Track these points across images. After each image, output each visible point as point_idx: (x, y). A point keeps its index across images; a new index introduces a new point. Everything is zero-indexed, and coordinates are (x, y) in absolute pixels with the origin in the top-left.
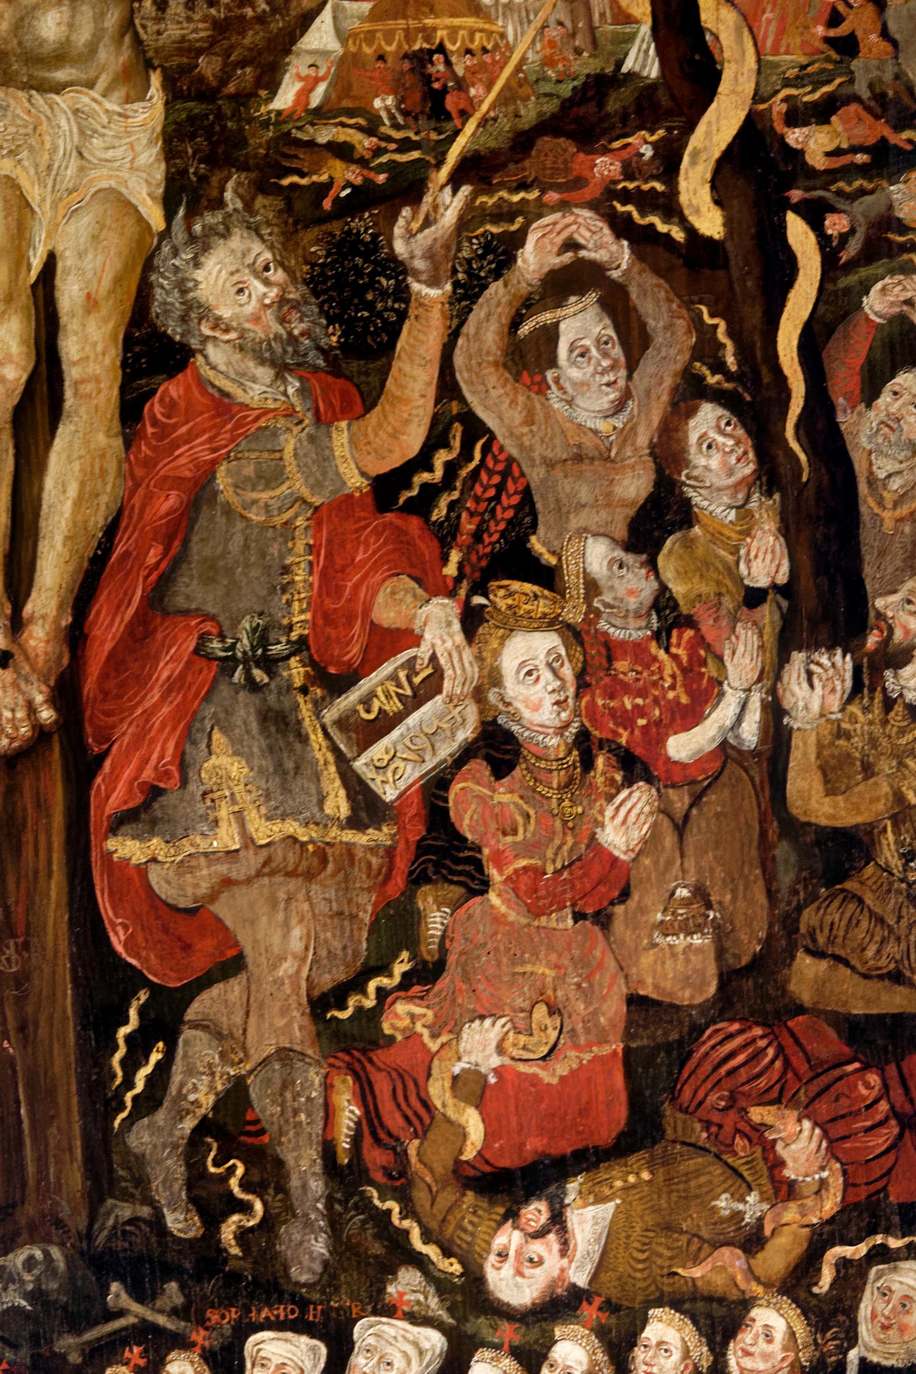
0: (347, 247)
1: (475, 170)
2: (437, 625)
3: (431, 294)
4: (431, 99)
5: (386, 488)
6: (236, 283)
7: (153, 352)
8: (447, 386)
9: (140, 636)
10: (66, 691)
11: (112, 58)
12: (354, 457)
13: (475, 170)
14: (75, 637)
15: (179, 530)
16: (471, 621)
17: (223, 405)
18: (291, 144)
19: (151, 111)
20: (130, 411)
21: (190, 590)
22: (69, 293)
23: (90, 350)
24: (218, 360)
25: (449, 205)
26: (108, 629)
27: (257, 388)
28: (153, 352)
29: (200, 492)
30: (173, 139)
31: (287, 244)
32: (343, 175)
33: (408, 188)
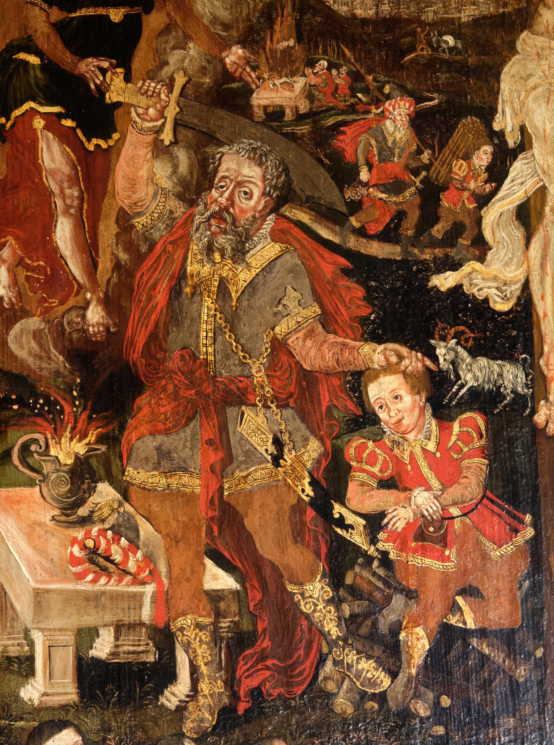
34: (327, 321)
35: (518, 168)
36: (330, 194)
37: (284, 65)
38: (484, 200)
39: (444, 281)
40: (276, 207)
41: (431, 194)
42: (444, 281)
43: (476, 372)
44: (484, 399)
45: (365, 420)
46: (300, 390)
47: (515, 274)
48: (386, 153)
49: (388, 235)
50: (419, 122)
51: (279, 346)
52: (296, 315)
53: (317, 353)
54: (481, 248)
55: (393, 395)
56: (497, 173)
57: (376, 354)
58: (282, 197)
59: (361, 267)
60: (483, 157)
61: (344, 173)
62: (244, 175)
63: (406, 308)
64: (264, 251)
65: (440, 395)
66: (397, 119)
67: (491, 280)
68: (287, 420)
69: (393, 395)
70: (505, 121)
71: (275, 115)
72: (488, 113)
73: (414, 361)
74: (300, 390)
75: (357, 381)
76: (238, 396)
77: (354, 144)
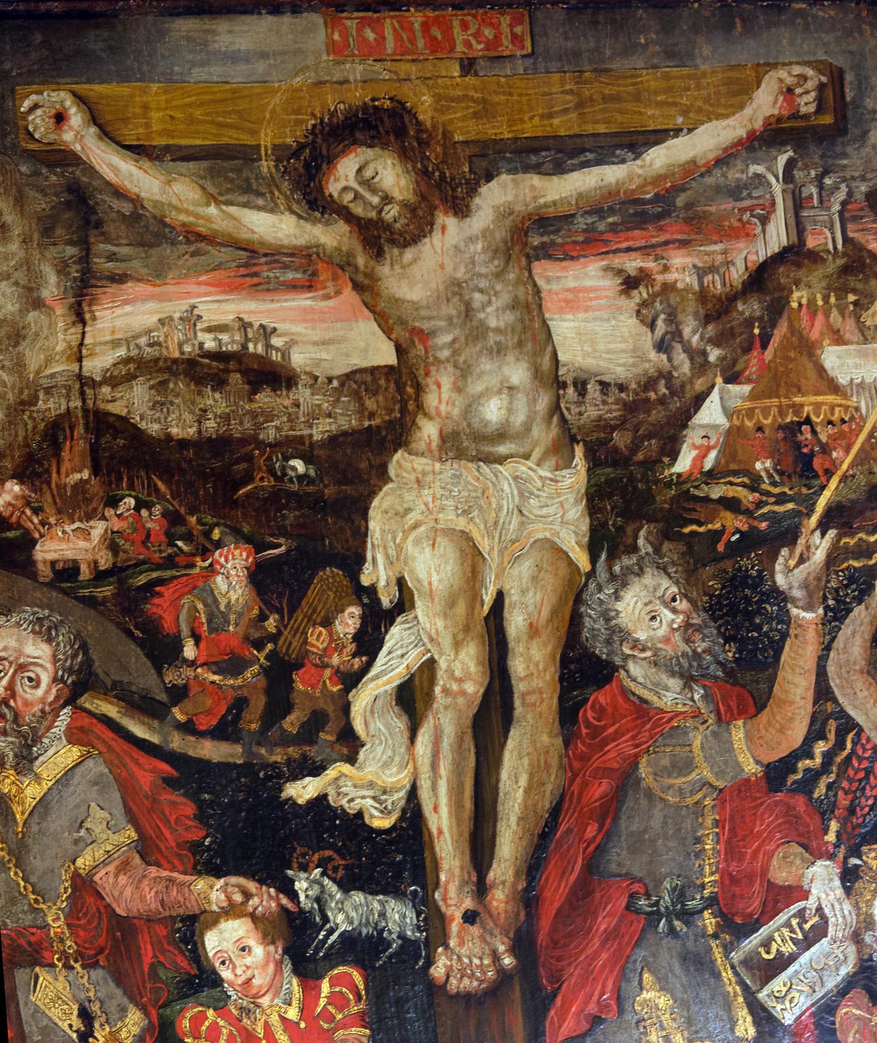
0: (738, 581)
1: (838, 517)
2: (822, 882)
3: (807, 617)
4: (802, 464)
5: (777, 773)
6: (648, 611)
7: (585, 669)
8: (823, 692)
9: (583, 896)
10: (523, 943)
11: (544, 435)
12: (747, 751)
13: (838, 517)
14: (529, 899)
15: (610, 810)
16: (849, 877)
17: (642, 710)
18: (687, 501)
19: (576, 476)
20: (568, 714)
21: (620, 858)
22: (516, 623)
23: (533, 665)
24: (637, 673)
25: (820, 546)
26: (556, 891)
27: (670, 695)
28: (585, 669)
29: (626, 779)
30: (595, 498)
31: (689, 579)
32: (732, 523)
33: (786, 534)
34: (147, 849)
35: (396, 634)
36: (144, 677)
37: (77, 505)
38: (352, 680)
39: (303, 790)
40: (71, 699)
41: (281, 673)
42: (303, 790)
43: (349, 912)
44: (362, 948)
45: (202, 980)
46: (111, 942)
47: (397, 778)
48: (217, 619)
49: (224, 732)
50: (260, 577)
51: (83, 885)
52: (104, 840)
53: (133, 893)
54: (350, 745)
55: (237, 947)
56: (369, 642)
57: (214, 891)
58: (79, 683)
59: (189, 774)
60: (349, 621)
61: (163, 650)
63: (253, 829)
64: (58, 756)
65: (300, 942)
66: (231, 575)
67: (369, 781)
68: (96, 984)
69: (237, 947)
70: (377, 573)
71: (66, 573)
72: (353, 561)
73: (265, 900)
74: (111, 942)
75: (191, 926)
76: (35, 954)
77: (177, 610)
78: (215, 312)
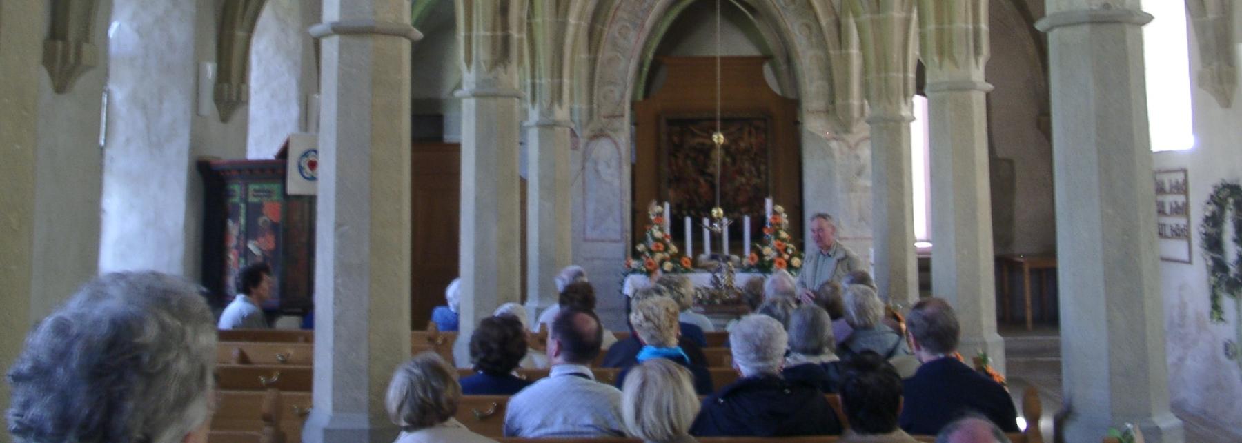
62: (689, 162)
63: (703, 173)
78: (701, 140)
